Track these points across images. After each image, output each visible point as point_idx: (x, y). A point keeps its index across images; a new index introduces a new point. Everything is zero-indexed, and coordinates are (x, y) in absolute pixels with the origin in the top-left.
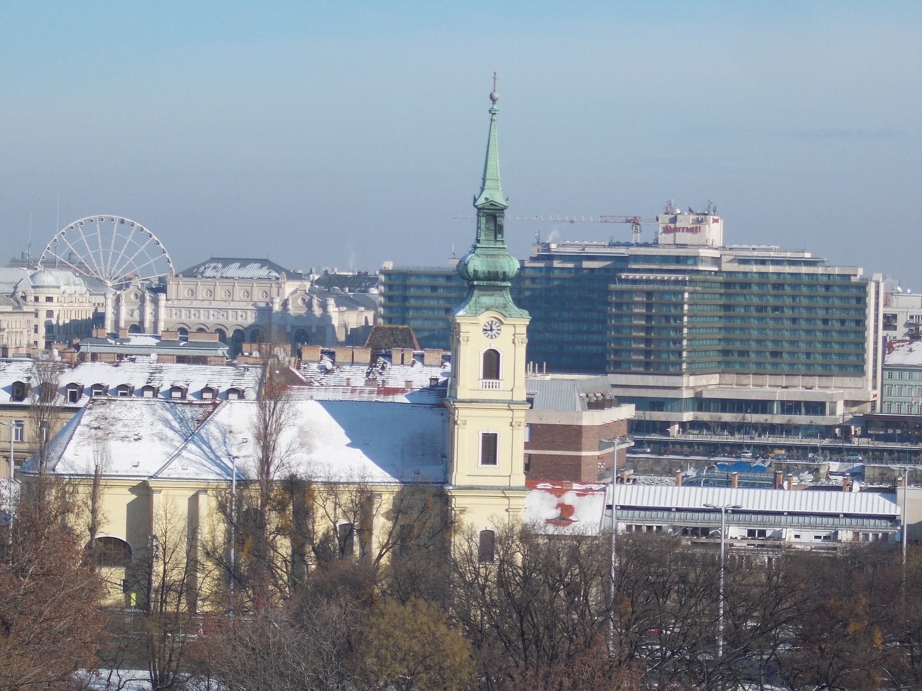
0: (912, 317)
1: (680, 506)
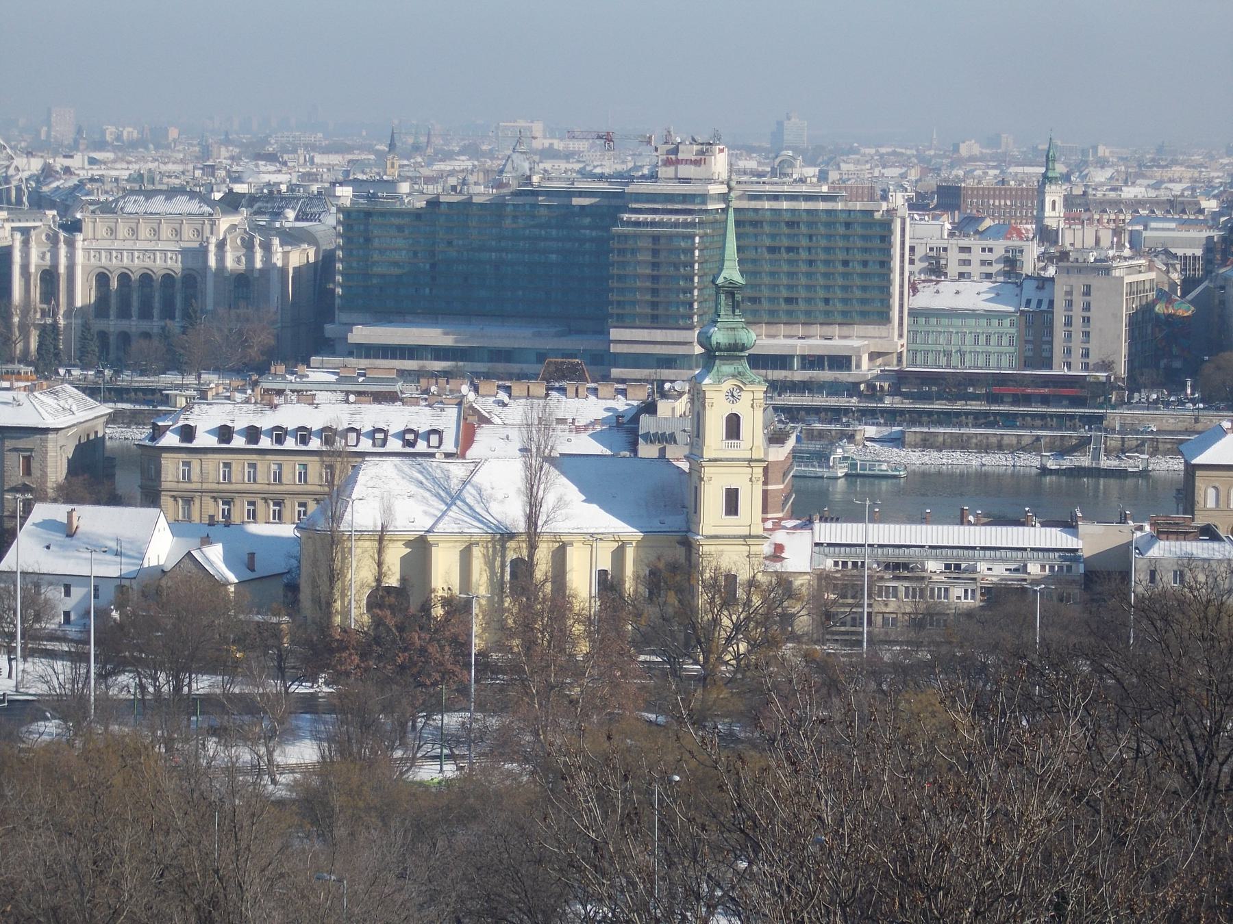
0: (931, 249)
1: (881, 542)
